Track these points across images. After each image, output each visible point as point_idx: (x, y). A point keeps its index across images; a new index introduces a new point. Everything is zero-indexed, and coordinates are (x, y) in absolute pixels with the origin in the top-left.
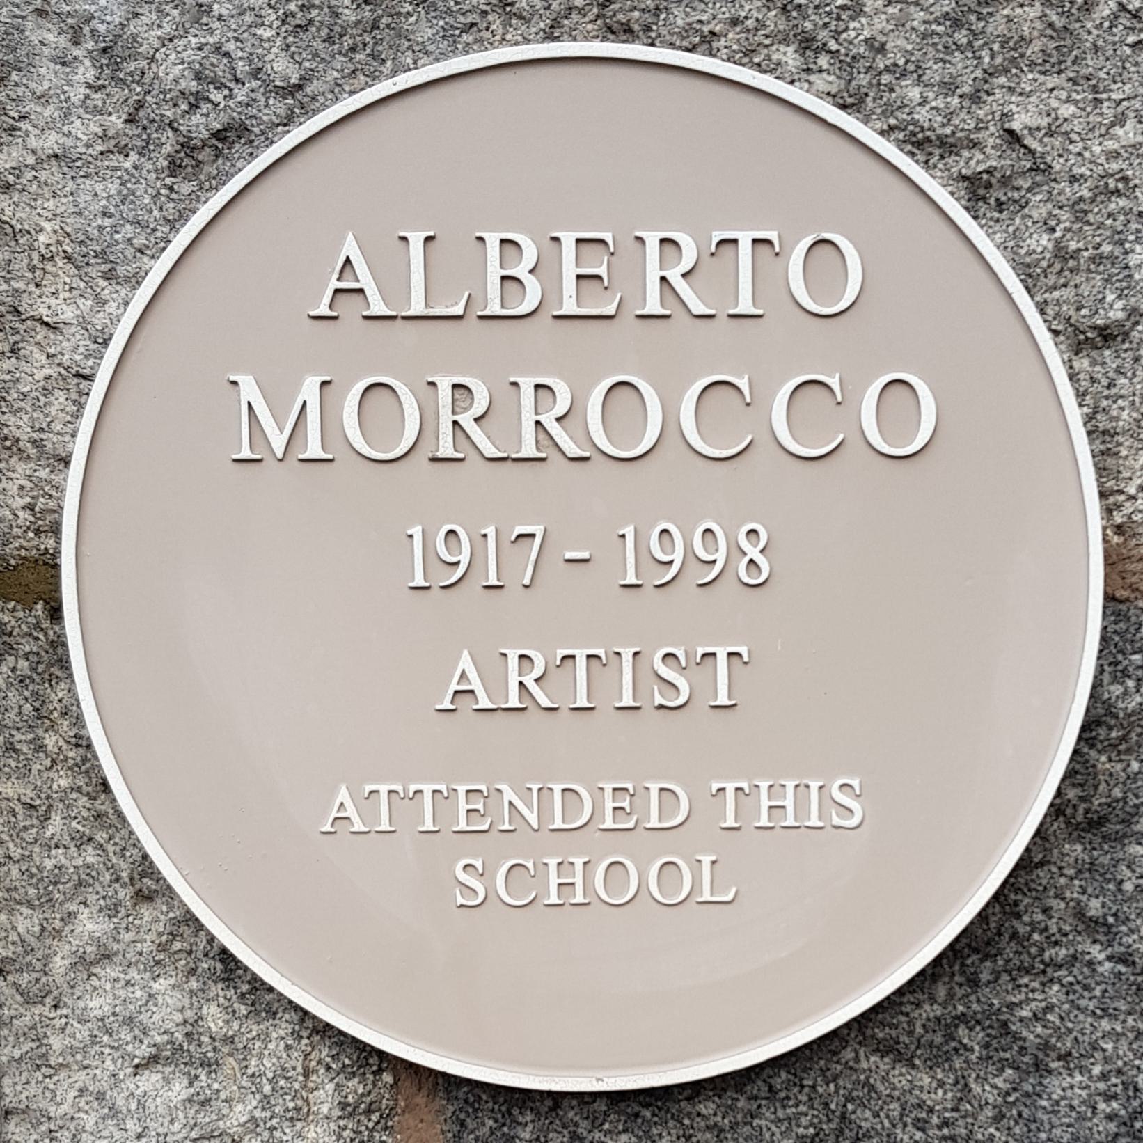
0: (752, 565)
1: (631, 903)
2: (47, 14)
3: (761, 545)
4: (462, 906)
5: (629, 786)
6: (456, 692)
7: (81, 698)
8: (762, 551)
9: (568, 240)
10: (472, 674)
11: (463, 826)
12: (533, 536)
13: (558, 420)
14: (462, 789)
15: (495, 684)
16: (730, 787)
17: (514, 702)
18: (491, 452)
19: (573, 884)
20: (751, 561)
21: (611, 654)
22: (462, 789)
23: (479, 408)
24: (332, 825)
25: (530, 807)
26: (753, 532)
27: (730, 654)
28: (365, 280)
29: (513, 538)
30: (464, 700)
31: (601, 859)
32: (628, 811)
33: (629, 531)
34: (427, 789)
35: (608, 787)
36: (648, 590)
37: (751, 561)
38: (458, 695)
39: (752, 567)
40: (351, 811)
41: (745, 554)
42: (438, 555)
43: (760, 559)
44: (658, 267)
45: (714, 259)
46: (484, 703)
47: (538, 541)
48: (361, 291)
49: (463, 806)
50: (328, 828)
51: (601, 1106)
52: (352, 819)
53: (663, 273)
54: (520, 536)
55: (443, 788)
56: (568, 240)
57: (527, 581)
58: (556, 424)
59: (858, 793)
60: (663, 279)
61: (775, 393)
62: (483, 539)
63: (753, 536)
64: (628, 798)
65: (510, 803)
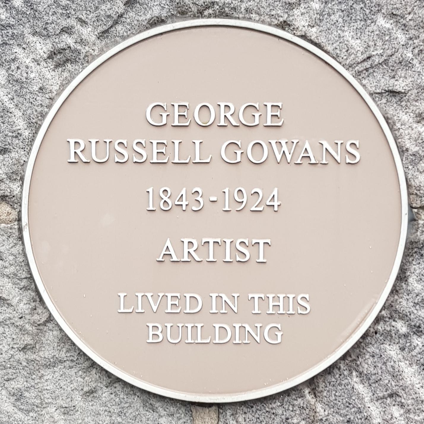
0: (165, 203)
1: (271, 345)
2: (87, 24)
3: (168, 196)
6: (164, 254)
7: (27, 253)
9: (269, 105)
11: (169, 310)
14: (169, 295)
17: (186, 258)
20: (165, 201)
21: (222, 241)
25: (155, 303)
26: (165, 191)
29: (193, 192)
30: (167, 258)
32: (178, 305)
34: (256, 296)
37: (165, 201)
38: (165, 255)
39: (166, 204)
43: (168, 201)
46: (175, 258)
55: (262, 296)
56: (269, 105)
63: (165, 192)
64: (177, 300)
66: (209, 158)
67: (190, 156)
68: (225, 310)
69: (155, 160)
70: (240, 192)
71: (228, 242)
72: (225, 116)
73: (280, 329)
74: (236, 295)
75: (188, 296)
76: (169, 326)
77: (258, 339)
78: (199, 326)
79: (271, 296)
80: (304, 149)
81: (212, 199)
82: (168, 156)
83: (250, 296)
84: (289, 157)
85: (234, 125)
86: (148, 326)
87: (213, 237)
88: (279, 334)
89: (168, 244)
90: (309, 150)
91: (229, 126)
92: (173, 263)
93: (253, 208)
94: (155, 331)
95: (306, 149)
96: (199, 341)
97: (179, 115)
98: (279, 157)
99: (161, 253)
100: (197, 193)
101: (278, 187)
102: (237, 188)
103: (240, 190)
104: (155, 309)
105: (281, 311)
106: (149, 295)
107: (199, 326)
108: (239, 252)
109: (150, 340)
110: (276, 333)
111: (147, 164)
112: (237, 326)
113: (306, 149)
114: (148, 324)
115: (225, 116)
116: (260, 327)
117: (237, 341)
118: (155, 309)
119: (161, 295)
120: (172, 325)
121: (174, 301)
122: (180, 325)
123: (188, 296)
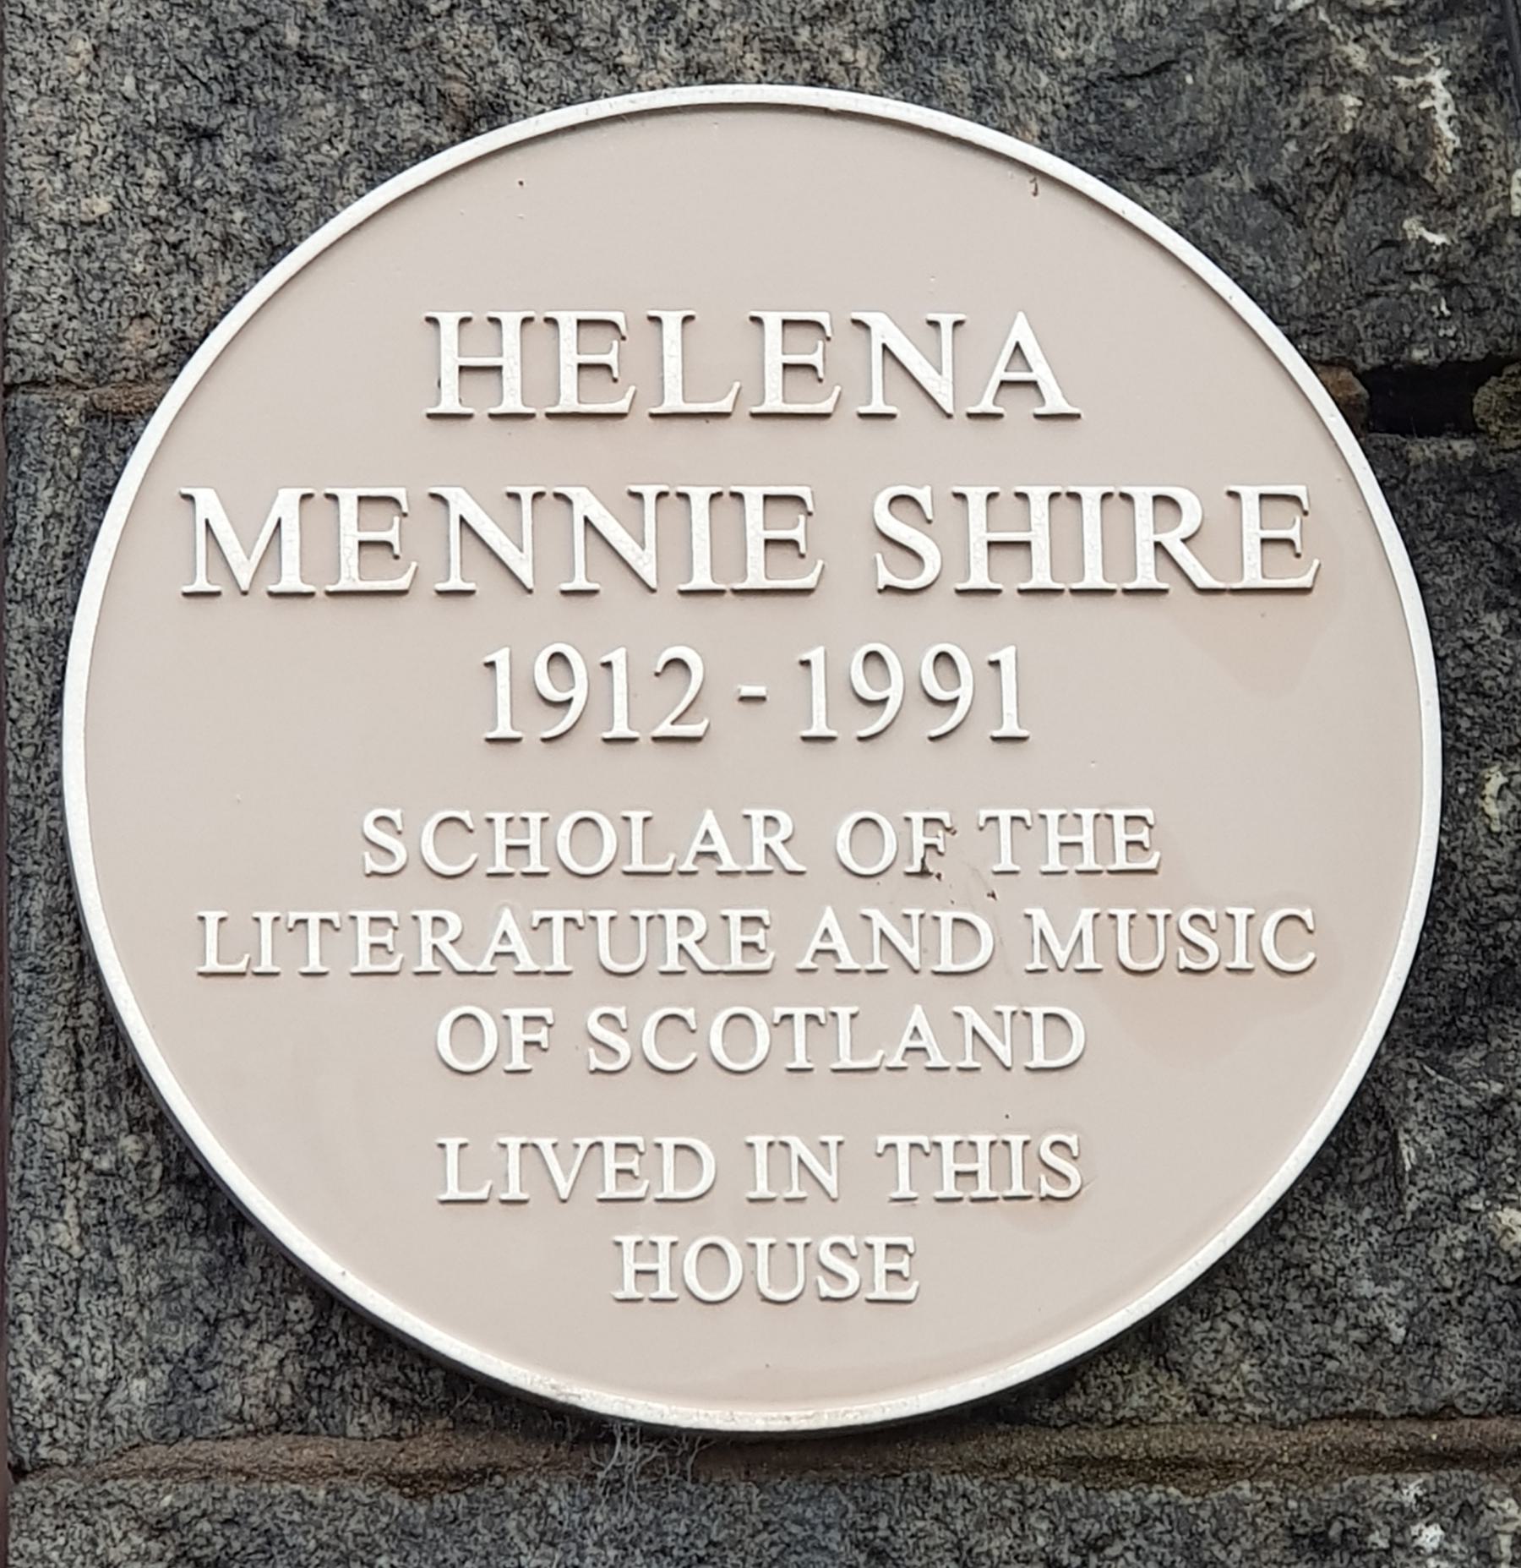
4: (597, 1071)
5: (392, 915)
14: (609, 1142)
15: (742, 848)
16: (558, 917)
24: (492, 962)
27: (1014, 818)
28: (1041, 372)
29: (659, 670)
35: (735, 915)
40: (517, 944)
42: (925, 692)
44: (1152, 529)
46: (728, 864)
48: (1033, 384)
49: (365, 938)
50: (807, 963)
52: (519, 955)
53: (1158, 538)
60: (1158, 545)
62: (991, 670)
65: (882, 934)
66: (829, 396)
67: (737, 385)
70: (942, 663)
74: (832, 1140)
75: (668, 1143)
79: (948, 1142)
80: (1009, 348)
81: (747, 691)
83: (883, 1140)
87: (811, 937)
89: (1021, 332)
90: (1031, 350)
93: (666, 729)
95: (1017, 346)
99: (989, 378)
100: (675, 671)
102: (862, 644)
104: (564, 1189)
106: (545, 1144)
113: (1017, 346)
116: (554, 1145)
118: (564, 1189)
119: (585, 1142)
121: (624, 1161)
123: (668, 1143)
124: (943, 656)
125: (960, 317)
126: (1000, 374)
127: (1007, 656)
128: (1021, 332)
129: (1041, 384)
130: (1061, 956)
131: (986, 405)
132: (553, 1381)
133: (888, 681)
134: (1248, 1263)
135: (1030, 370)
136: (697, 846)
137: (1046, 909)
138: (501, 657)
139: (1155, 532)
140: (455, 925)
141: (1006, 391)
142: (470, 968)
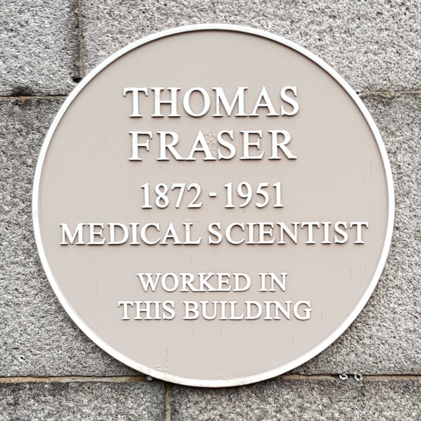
3: (165, 192)
8: (166, 194)
10: (173, 232)
12: (180, 188)
13: (174, 146)
14: (220, 275)
18: (178, 157)
19: (146, 312)
20: (161, 198)
22: (220, 275)
23: (174, 142)
26: (161, 187)
28: (269, 104)
29: (172, 188)
31: (296, 302)
33: (229, 185)
36: (237, 209)
37: (161, 198)
39: (162, 201)
41: (158, 195)
42: (238, 194)
43: (165, 198)
45: (124, 98)
46: (177, 241)
47: (182, 190)
49: (221, 281)
51: (179, 386)
53: (167, 146)
54: (175, 188)
56: (246, 133)
57: (177, 206)
58: (173, 148)
59: (153, 290)
61: (220, 131)
63: (161, 188)
68: (274, 288)
69: (246, 156)
70: (244, 187)
71: (326, 224)
72: (167, 148)
73: (309, 306)
75: (237, 275)
76: (204, 303)
77: (288, 315)
78: (233, 303)
81: (212, 194)
82: (263, 152)
84: (153, 287)
85: (290, 157)
86: (184, 304)
88: (308, 310)
89: (264, 93)
91: (172, 160)
92: (78, 246)
93: (191, 205)
94: (191, 308)
95: (199, 142)
96: (233, 317)
97: (139, 147)
98: (146, 287)
100: (193, 190)
101: (280, 182)
103: (244, 185)
105: (148, 317)
107: (233, 303)
108: (212, 235)
109: (187, 317)
110: (305, 310)
111: (236, 160)
112: (268, 303)
113: (199, 142)
114: (185, 302)
115: (167, 148)
117: (268, 317)
120: (207, 302)
122: (215, 302)
124: (244, 185)
125: (246, 88)
126: (258, 105)
127: (278, 185)
128: (264, 93)
129: (269, 107)
130: (229, 110)
131: (254, 114)
132: (119, 379)
133: (247, 192)
134: (324, 352)
135: (202, 147)
136: (167, 236)
137: (175, 183)
138: (146, 186)
139: (166, 144)
140: (192, 278)
141: (196, 153)
142: (196, 290)
